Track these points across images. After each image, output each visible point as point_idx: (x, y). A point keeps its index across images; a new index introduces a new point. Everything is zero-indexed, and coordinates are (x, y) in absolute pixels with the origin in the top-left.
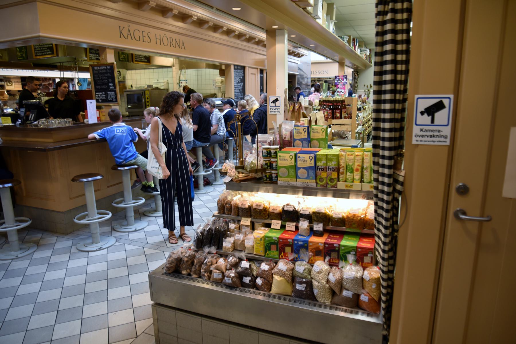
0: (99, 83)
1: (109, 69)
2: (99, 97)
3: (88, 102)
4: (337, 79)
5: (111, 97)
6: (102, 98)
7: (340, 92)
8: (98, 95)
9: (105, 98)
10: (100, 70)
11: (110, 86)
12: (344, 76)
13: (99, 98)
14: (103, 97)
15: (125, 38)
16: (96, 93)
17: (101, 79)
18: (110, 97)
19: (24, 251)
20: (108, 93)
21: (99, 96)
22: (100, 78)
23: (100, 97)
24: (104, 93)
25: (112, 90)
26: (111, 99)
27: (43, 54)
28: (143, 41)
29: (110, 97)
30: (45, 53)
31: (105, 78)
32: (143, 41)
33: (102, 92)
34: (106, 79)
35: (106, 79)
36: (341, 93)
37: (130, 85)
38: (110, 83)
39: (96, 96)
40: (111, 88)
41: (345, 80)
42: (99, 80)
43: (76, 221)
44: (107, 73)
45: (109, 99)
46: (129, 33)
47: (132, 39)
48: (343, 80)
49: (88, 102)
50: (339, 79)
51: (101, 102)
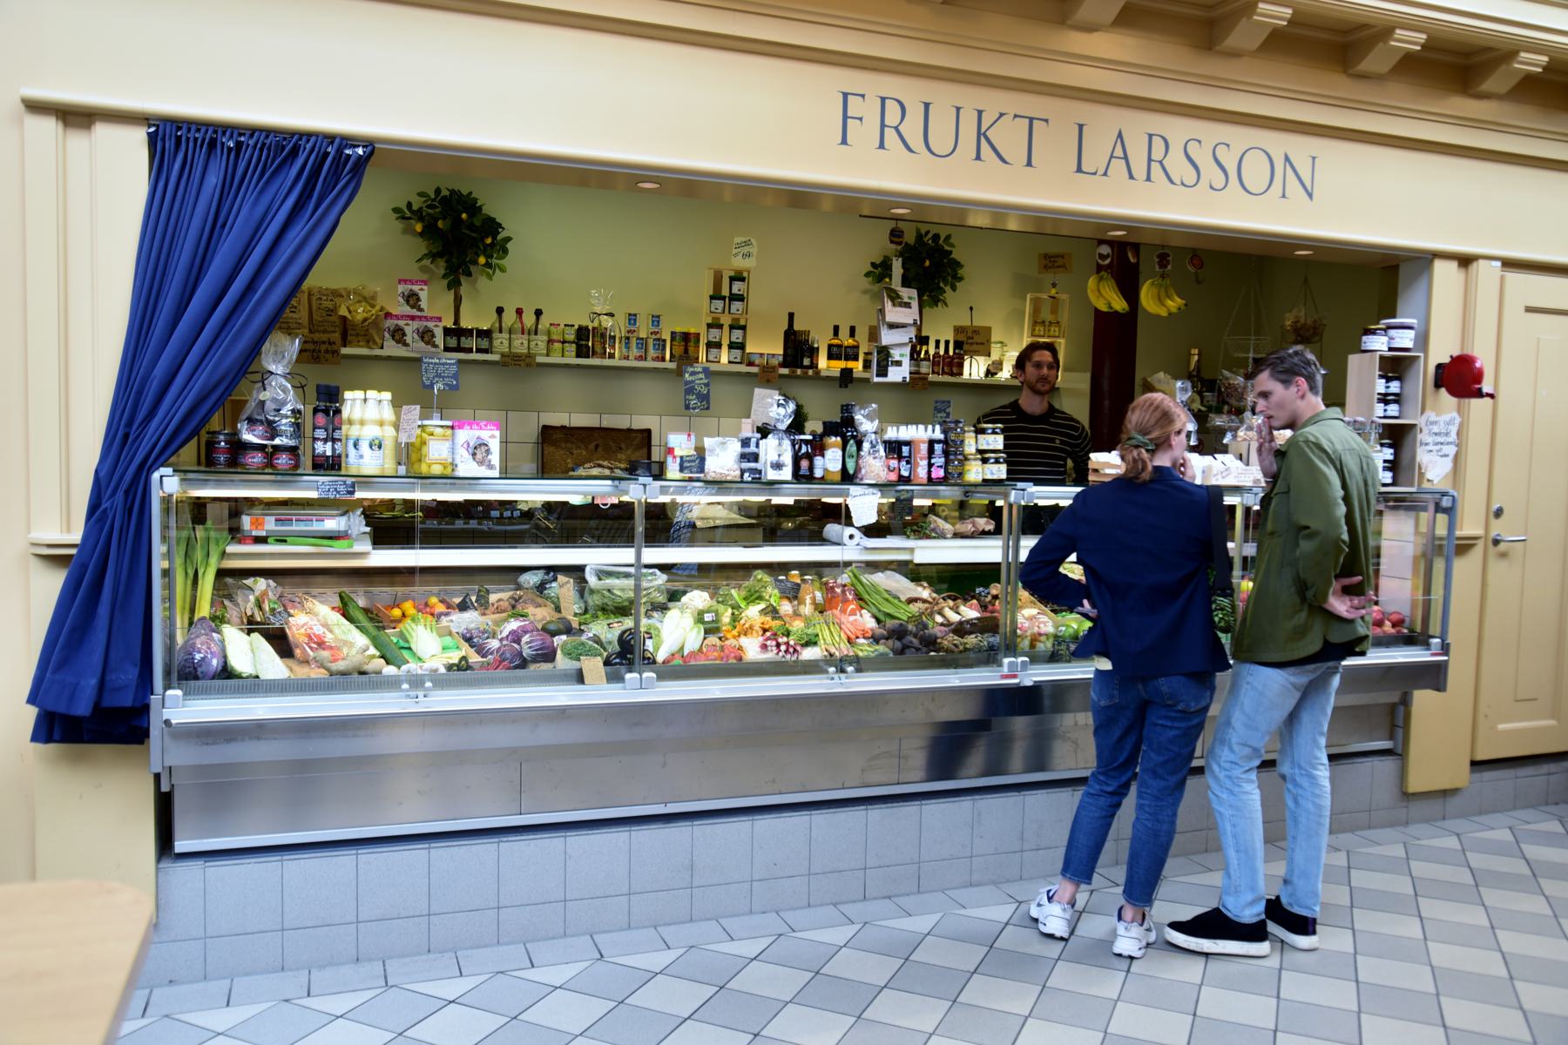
15: (1171, 181)
28: (1079, 170)
32: (1079, 170)
46: (1119, 152)
47: (1131, 177)
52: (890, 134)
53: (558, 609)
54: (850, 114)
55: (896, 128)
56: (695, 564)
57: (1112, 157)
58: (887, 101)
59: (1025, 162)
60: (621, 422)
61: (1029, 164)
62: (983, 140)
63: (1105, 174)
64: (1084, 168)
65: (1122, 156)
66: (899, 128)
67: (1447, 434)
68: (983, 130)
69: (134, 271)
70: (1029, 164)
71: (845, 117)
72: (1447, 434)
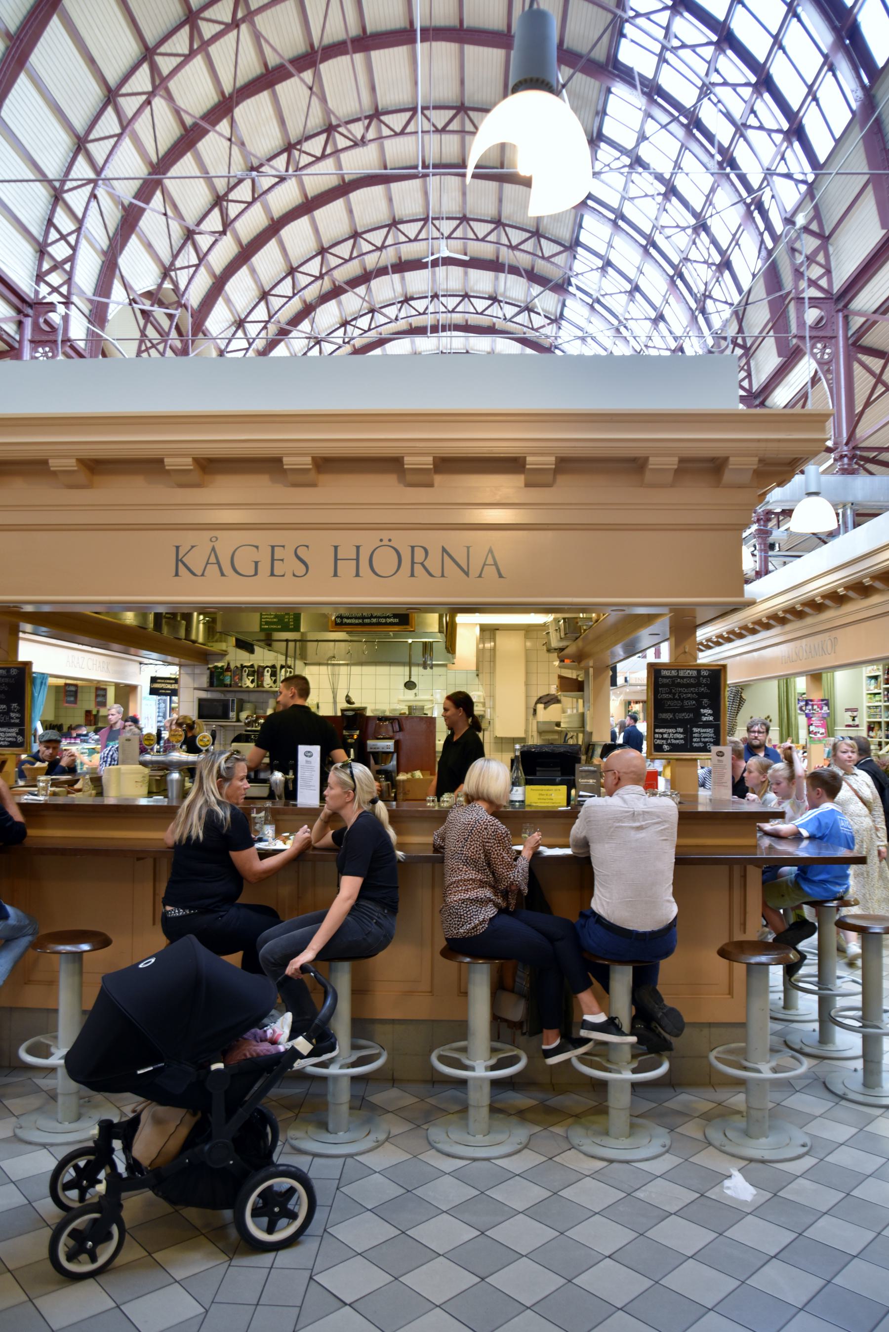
0: (669, 706)
1: (704, 677)
2: (663, 739)
3: (302, 749)
4: (810, 707)
5: (703, 740)
6: (674, 741)
7: (815, 733)
8: (662, 734)
9: (682, 742)
10: (678, 677)
11: (704, 715)
12: (822, 700)
13: (664, 741)
14: (677, 739)
16: (657, 730)
17: (677, 696)
18: (698, 740)
19: (218, 1262)
20: (695, 730)
21: (665, 736)
22: (674, 694)
23: (667, 739)
24: (680, 730)
25: (706, 725)
26: (701, 745)
27: (367, 621)
29: (698, 740)
30: (374, 620)
31: (689, 695)
32: (272, 574)
33: (675, 727)
34: (693, 699)
35: (693, 699)
36: (819, 735)
37: (315, 702)
38: (704, 708)
39: (657, 736)
40: (704, 719)
41: (825, 708)
42: (670, 699)
43: (712, 1056)
44: (698, 685)
45: (695, 745)
46: (213, 559)
47: (223, 574)
48: (821, 709)
49: (302, 749)
50: (813, 705)
51: (667, 751)
52: (418, 568)
53: (759, 575)
54: (355, 562)
55: (422, 564)
56: (590, 854)
57: (207, 563)
58: (276, 548)
59: (174, 574)
60: (497, 821)
61: (335, 575)
62: (180, 564)
63: (203, 575)
64: (276, 573)
65: (215, 561)
66: (425, 563)
67: (488, 631)
68: (180, 557)
69: (879, 273)
70: (335, 575)
71: (273, 560)
72: (488, 631)
